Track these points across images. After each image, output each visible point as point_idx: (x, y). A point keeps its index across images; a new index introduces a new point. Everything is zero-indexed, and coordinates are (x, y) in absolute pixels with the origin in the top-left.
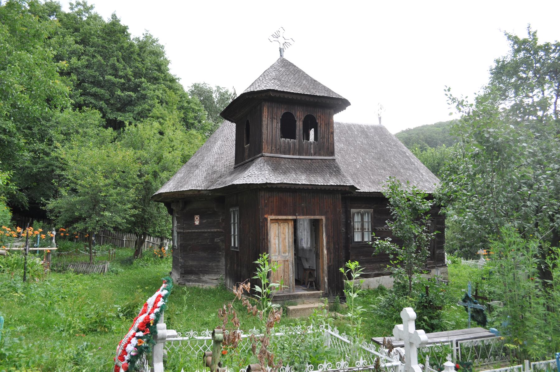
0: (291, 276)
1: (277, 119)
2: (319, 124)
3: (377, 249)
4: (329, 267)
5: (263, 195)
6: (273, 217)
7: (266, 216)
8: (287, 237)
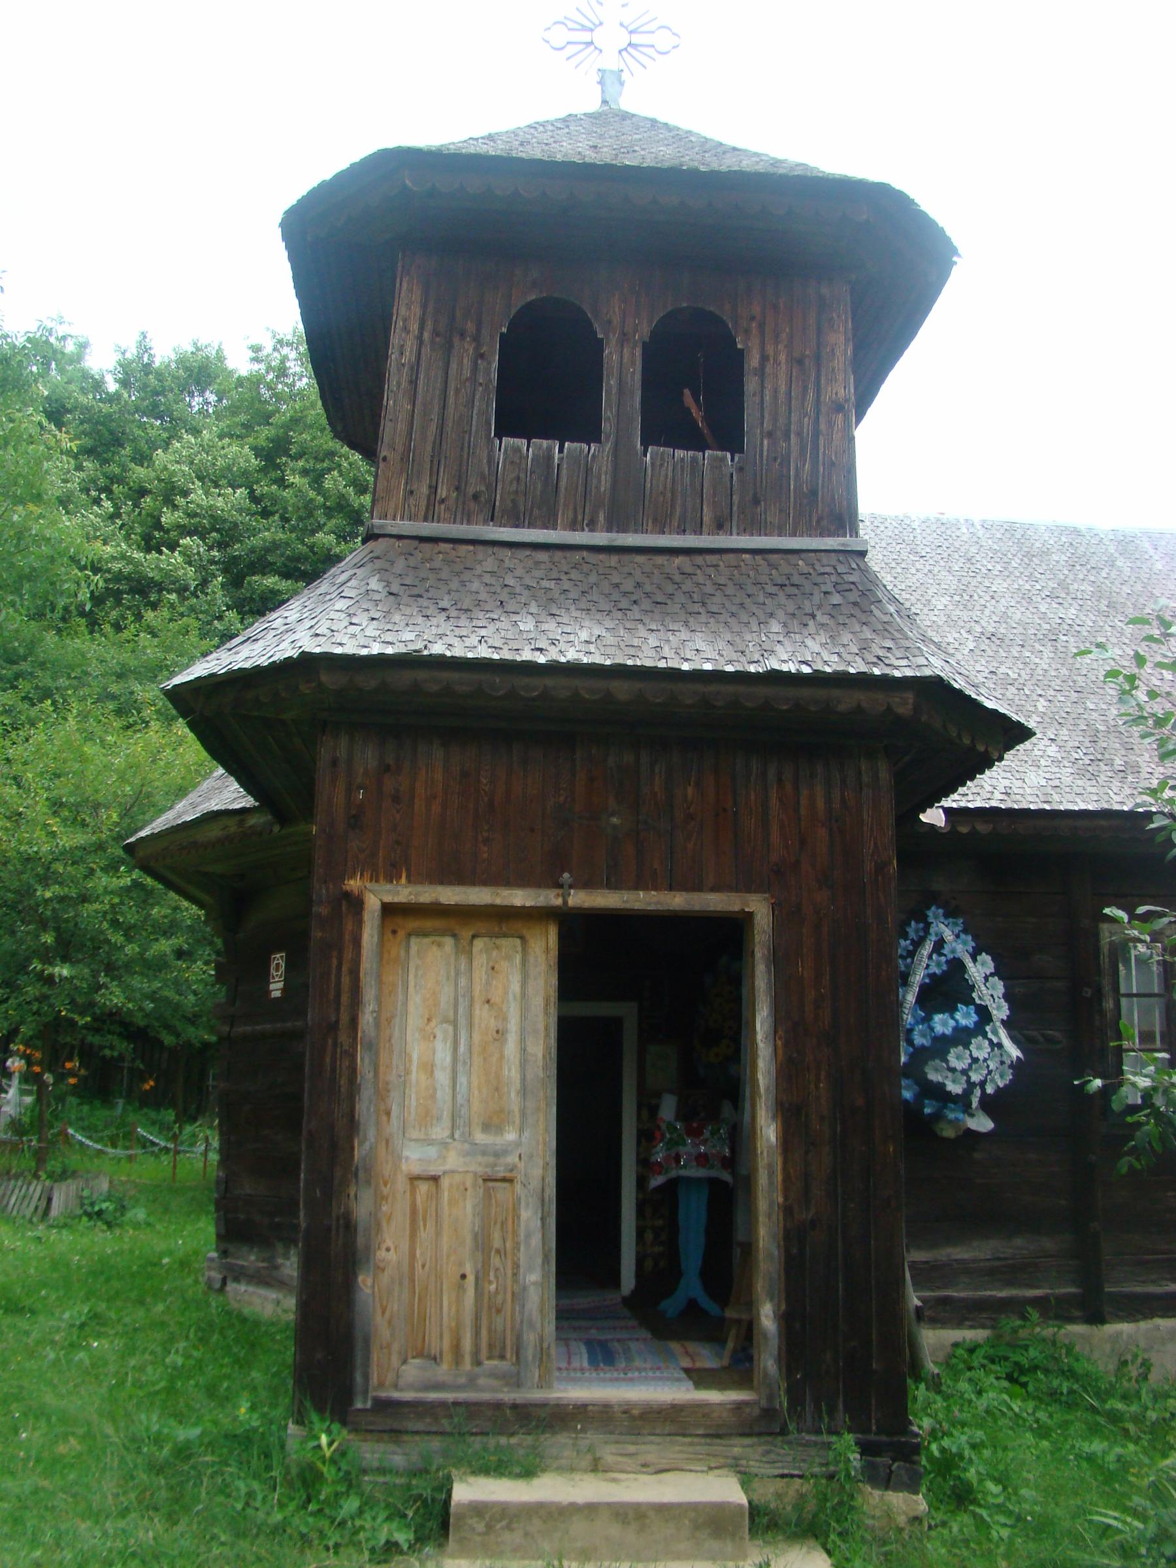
0: (534, 1277)
1: (476, 339)
2: (753, 361)
3: (1151, 1126)
4: (794, 1237)
5: (342, 753)
6: (403, 893)
7: (353, 884)
8: (513, 1026)
